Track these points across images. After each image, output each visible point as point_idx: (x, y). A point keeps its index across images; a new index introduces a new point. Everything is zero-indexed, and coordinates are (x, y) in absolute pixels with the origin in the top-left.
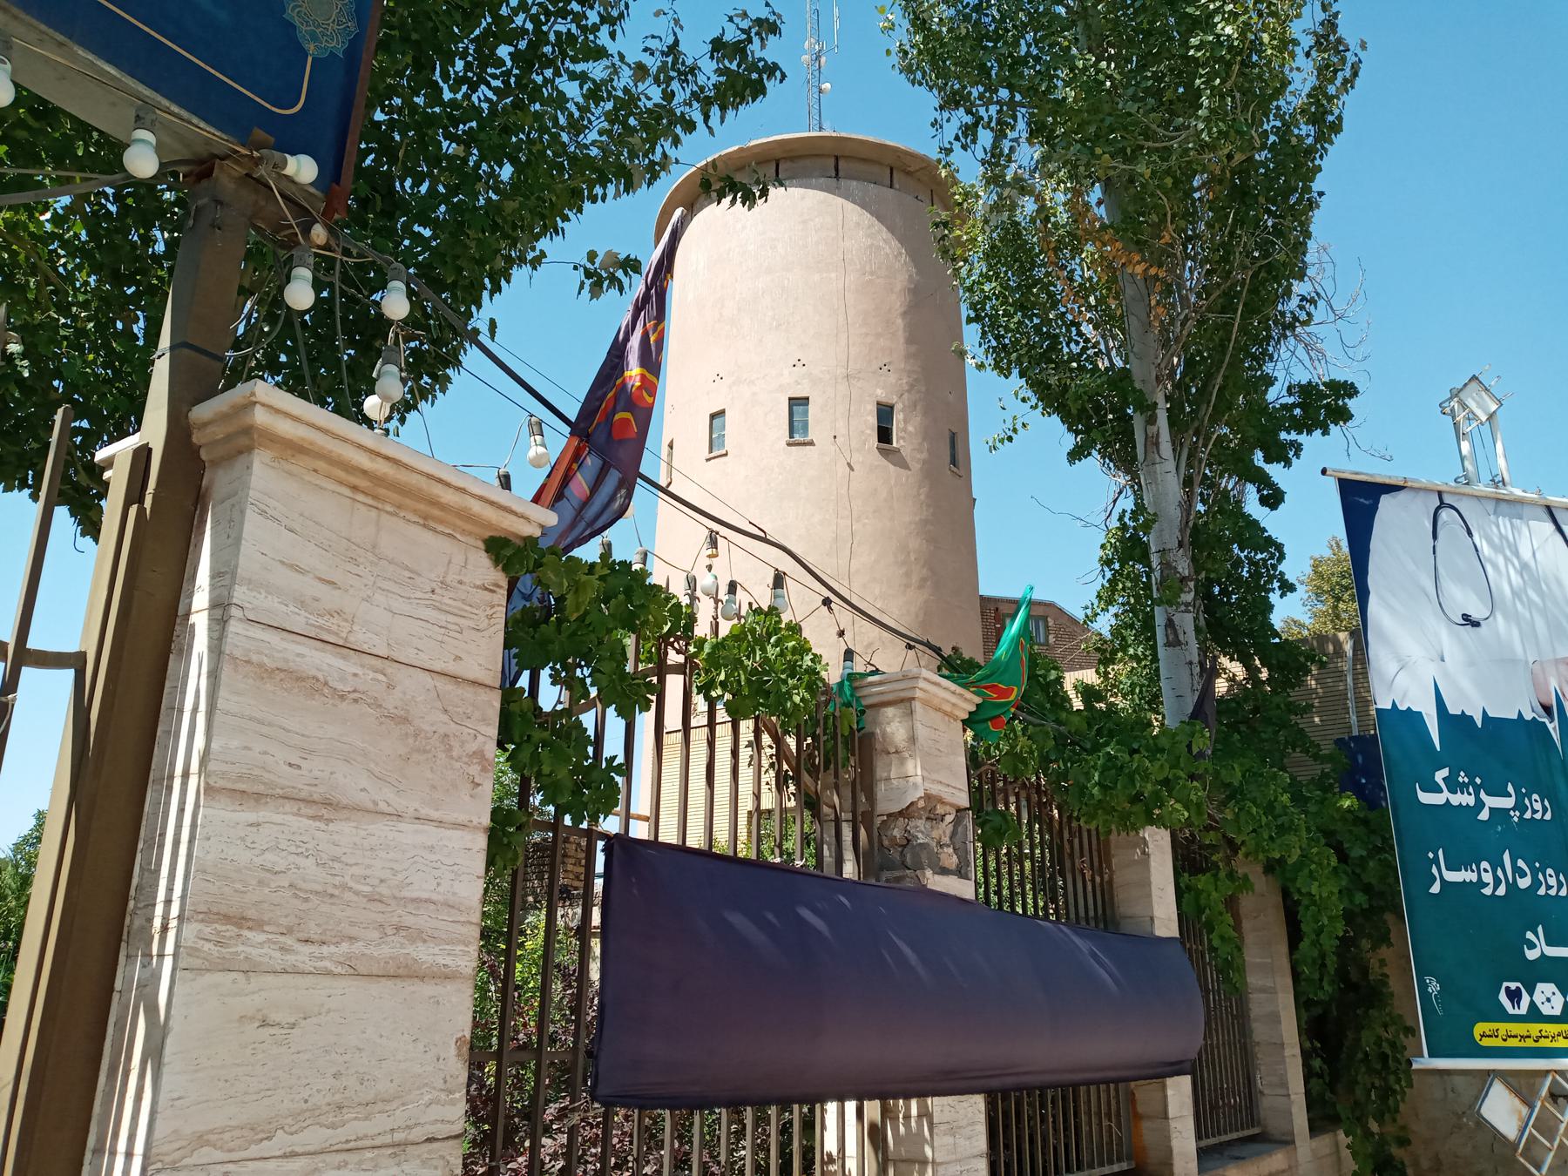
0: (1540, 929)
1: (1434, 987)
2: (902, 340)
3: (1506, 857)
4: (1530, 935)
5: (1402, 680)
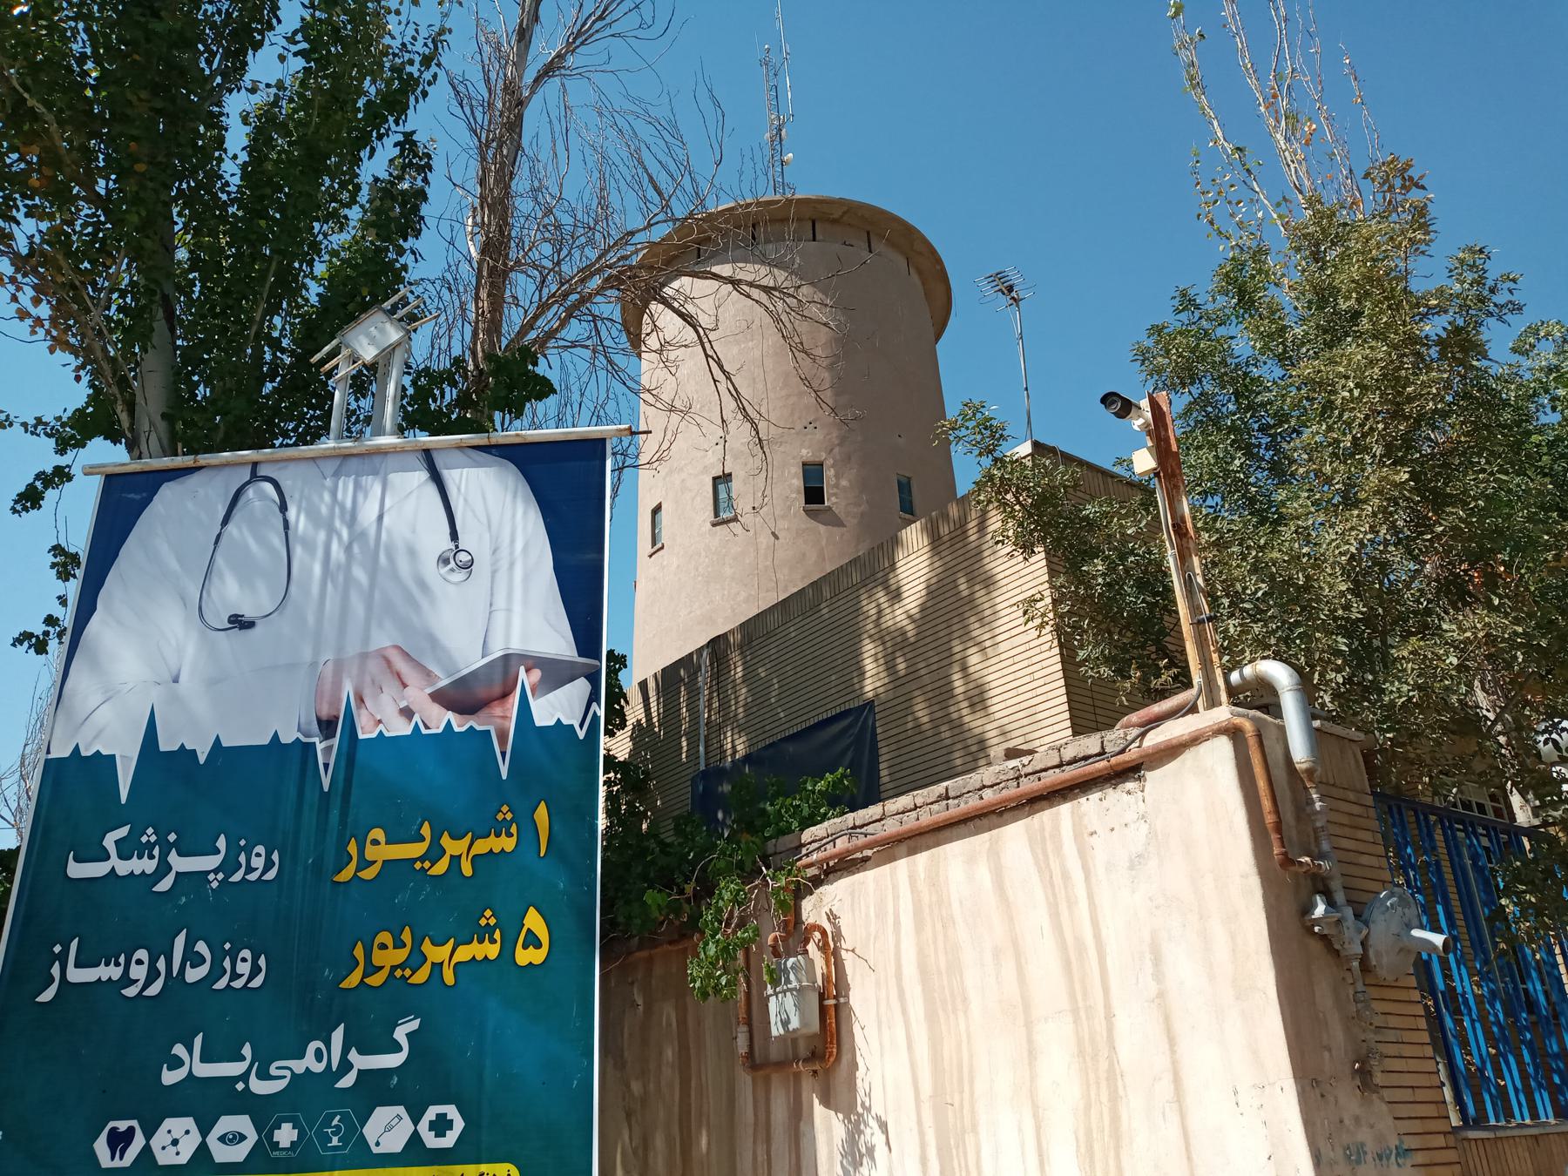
4: (179, 1050)
5: (105, 715)
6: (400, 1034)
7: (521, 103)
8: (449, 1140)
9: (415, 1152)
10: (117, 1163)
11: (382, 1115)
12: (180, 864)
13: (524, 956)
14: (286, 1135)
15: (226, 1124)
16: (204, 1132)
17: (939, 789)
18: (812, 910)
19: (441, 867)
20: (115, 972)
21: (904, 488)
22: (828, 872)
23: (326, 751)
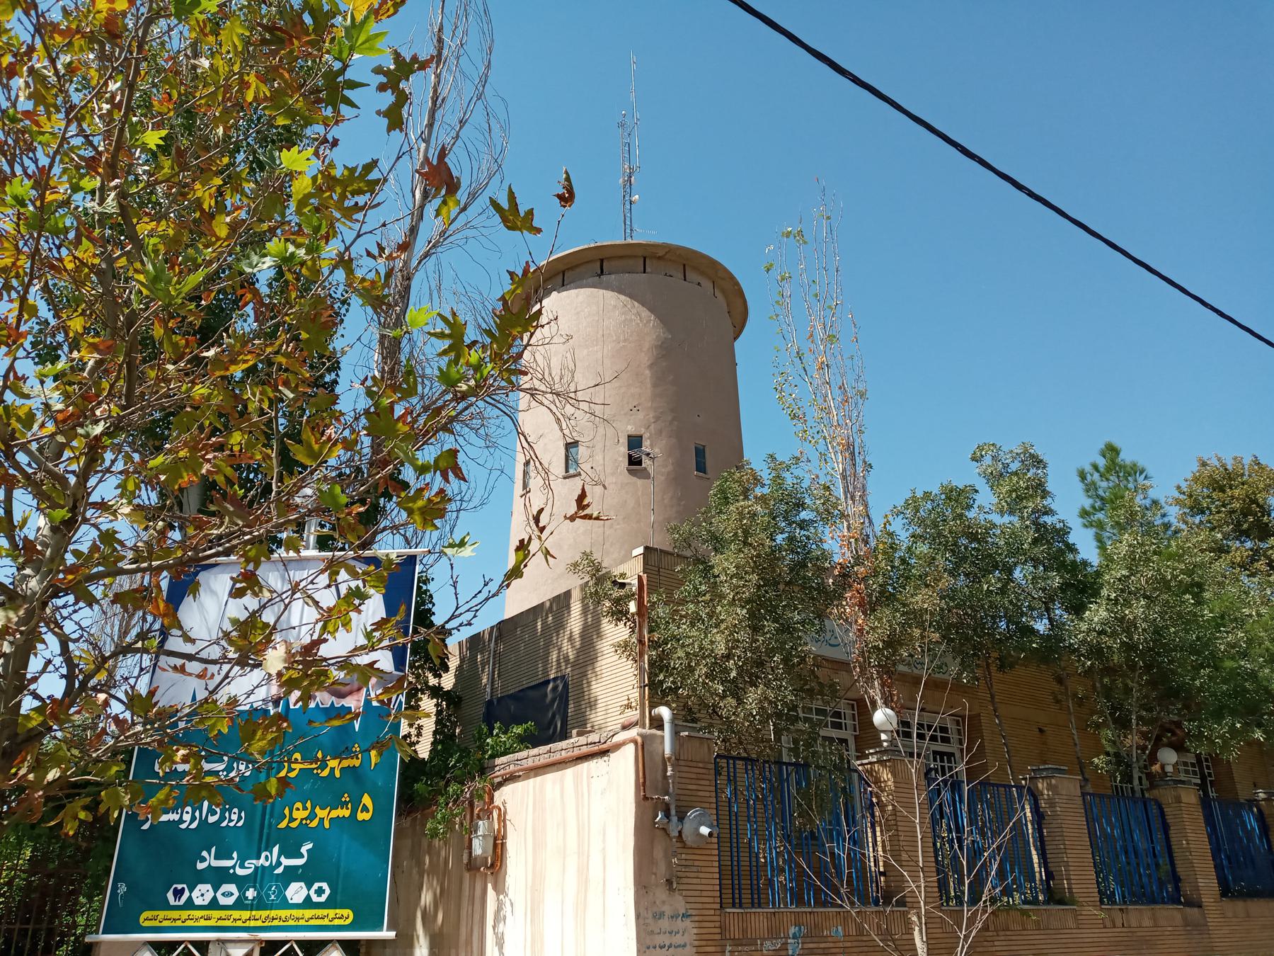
0: (213, 850)
1: (123, 888)
2: (649, 386)
3: (206, 804)
4: (204, 853)
6: (304, 850)
7: (409, 279)
8: (323, 898)
9: (308, 903)
10: (177, 903)
11: (294, 886)
13: (362, 816)
14: (251, 894)
16: (216, 891)
17: (547, 747)
18: (501, 796)
19: (326, 773)
20: (176, 817)
21: (700, 453)
22: (506, 780)
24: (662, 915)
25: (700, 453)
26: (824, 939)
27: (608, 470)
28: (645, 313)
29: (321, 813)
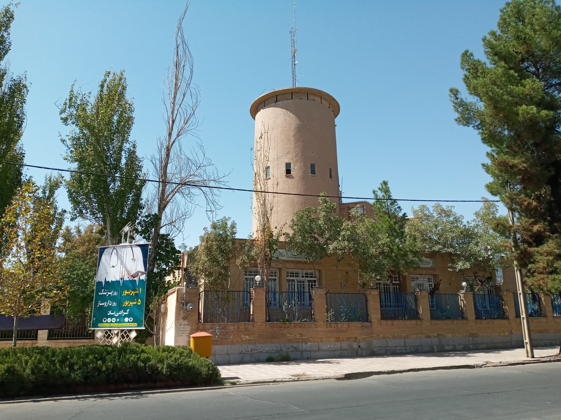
9: (129, 322)
12: (109, 293)
13: (139, 304)
14: (118, 320)
15: (113, 319)
21: (313, 166)
23: (121, 282)
24: (181, 325)
25: (313, 166)
26: (227, 329)
27: (279, 177)
28: (292, 115)
29: (131, 303)
